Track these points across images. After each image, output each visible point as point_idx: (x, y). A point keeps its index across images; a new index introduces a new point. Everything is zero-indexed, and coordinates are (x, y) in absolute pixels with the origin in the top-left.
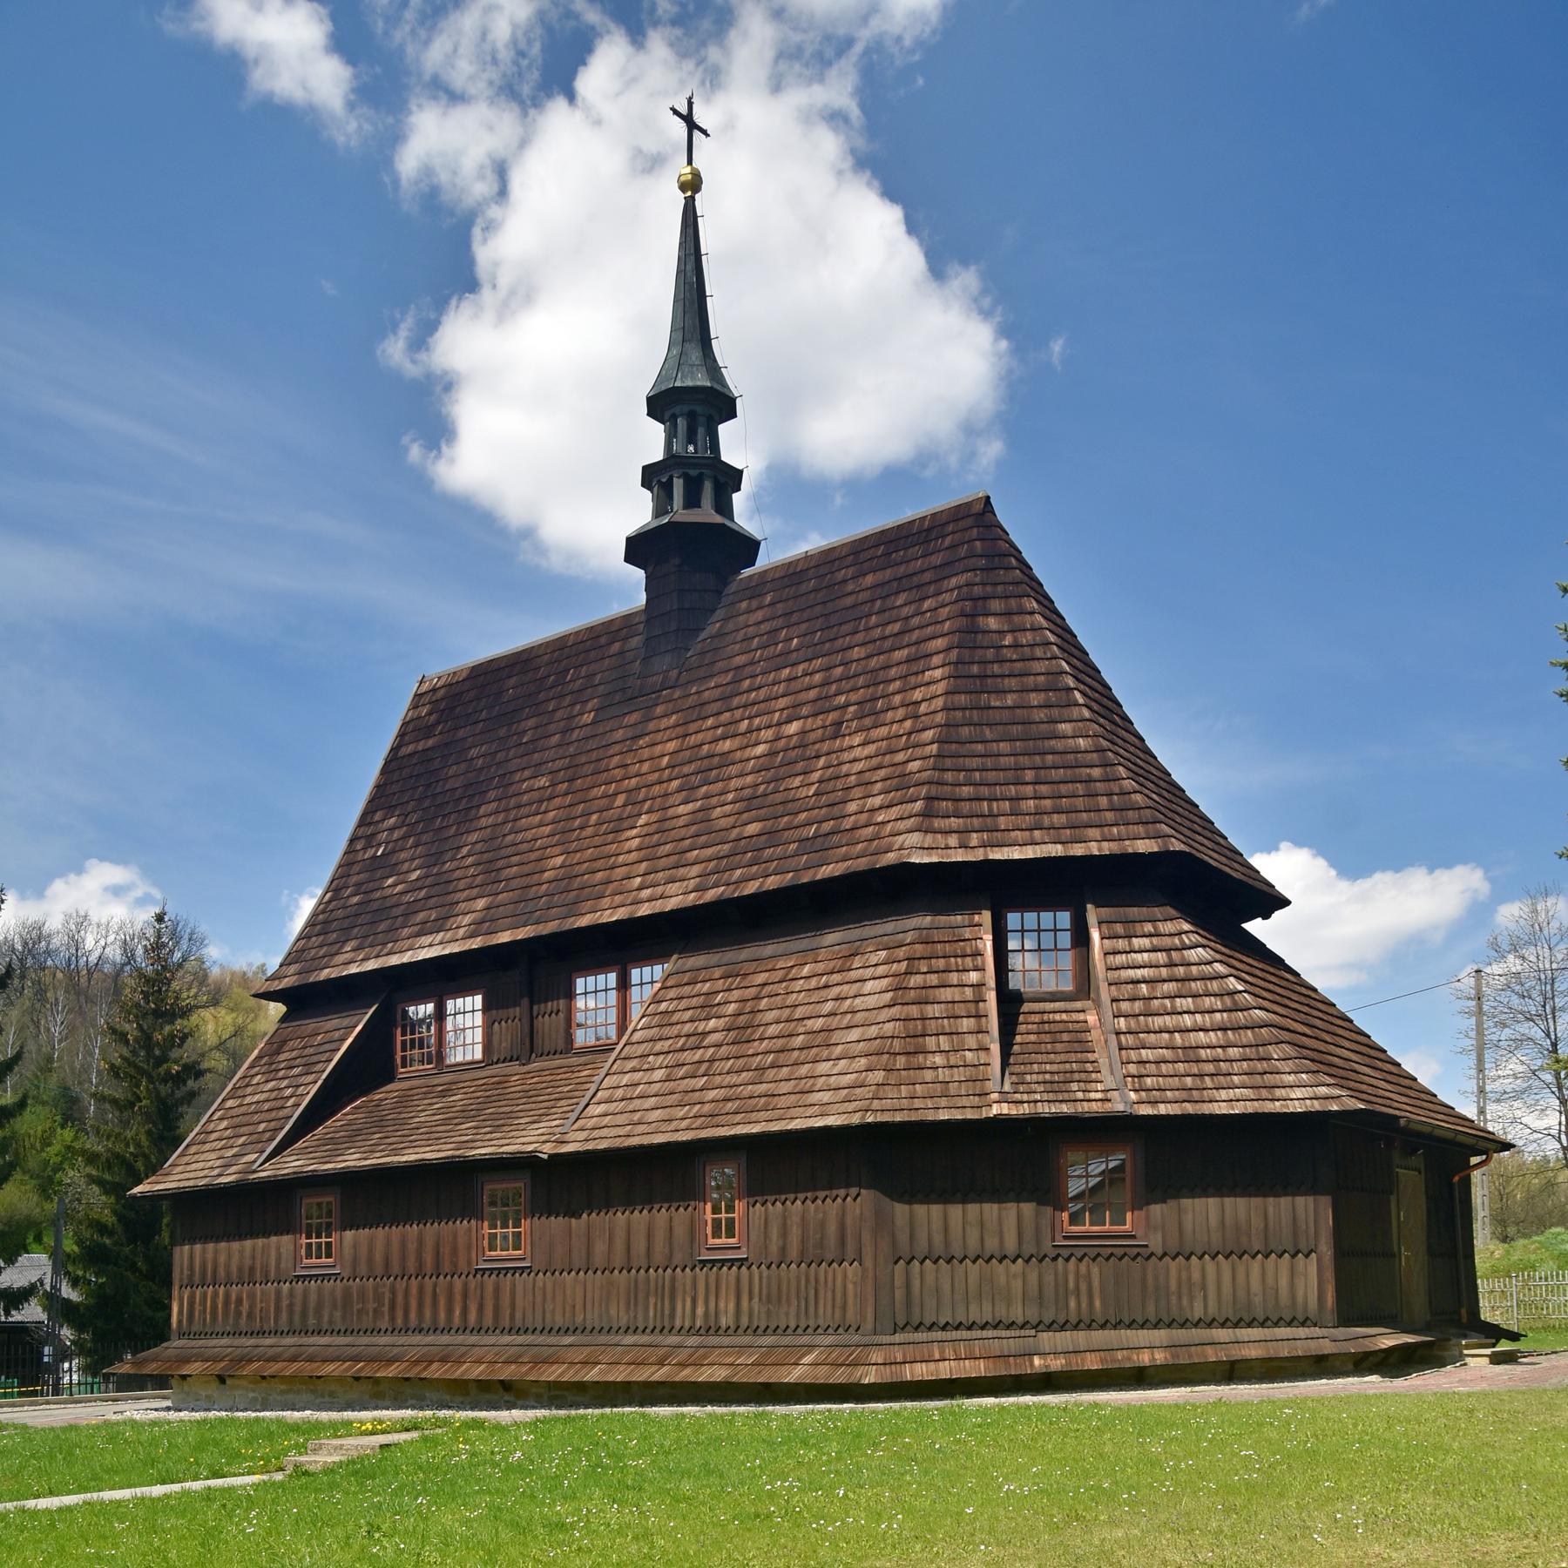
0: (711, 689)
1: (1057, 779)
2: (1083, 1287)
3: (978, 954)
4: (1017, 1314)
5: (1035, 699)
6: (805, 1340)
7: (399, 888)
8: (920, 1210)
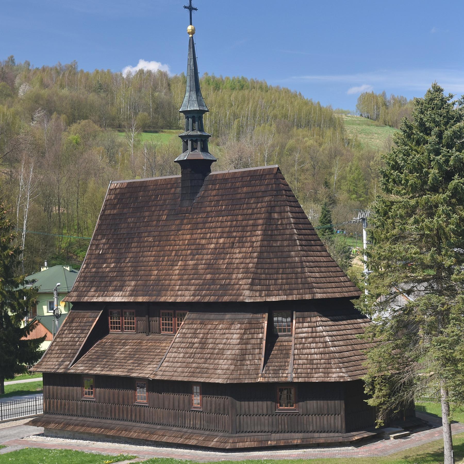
0: (200, 217)
1: (288, 272)
2: (283, 422)
3: (263, 328)
4: (267, 429)
5: (285, 243)
6: (216, 433)
7: (108, 269)
8: (243, 403)
